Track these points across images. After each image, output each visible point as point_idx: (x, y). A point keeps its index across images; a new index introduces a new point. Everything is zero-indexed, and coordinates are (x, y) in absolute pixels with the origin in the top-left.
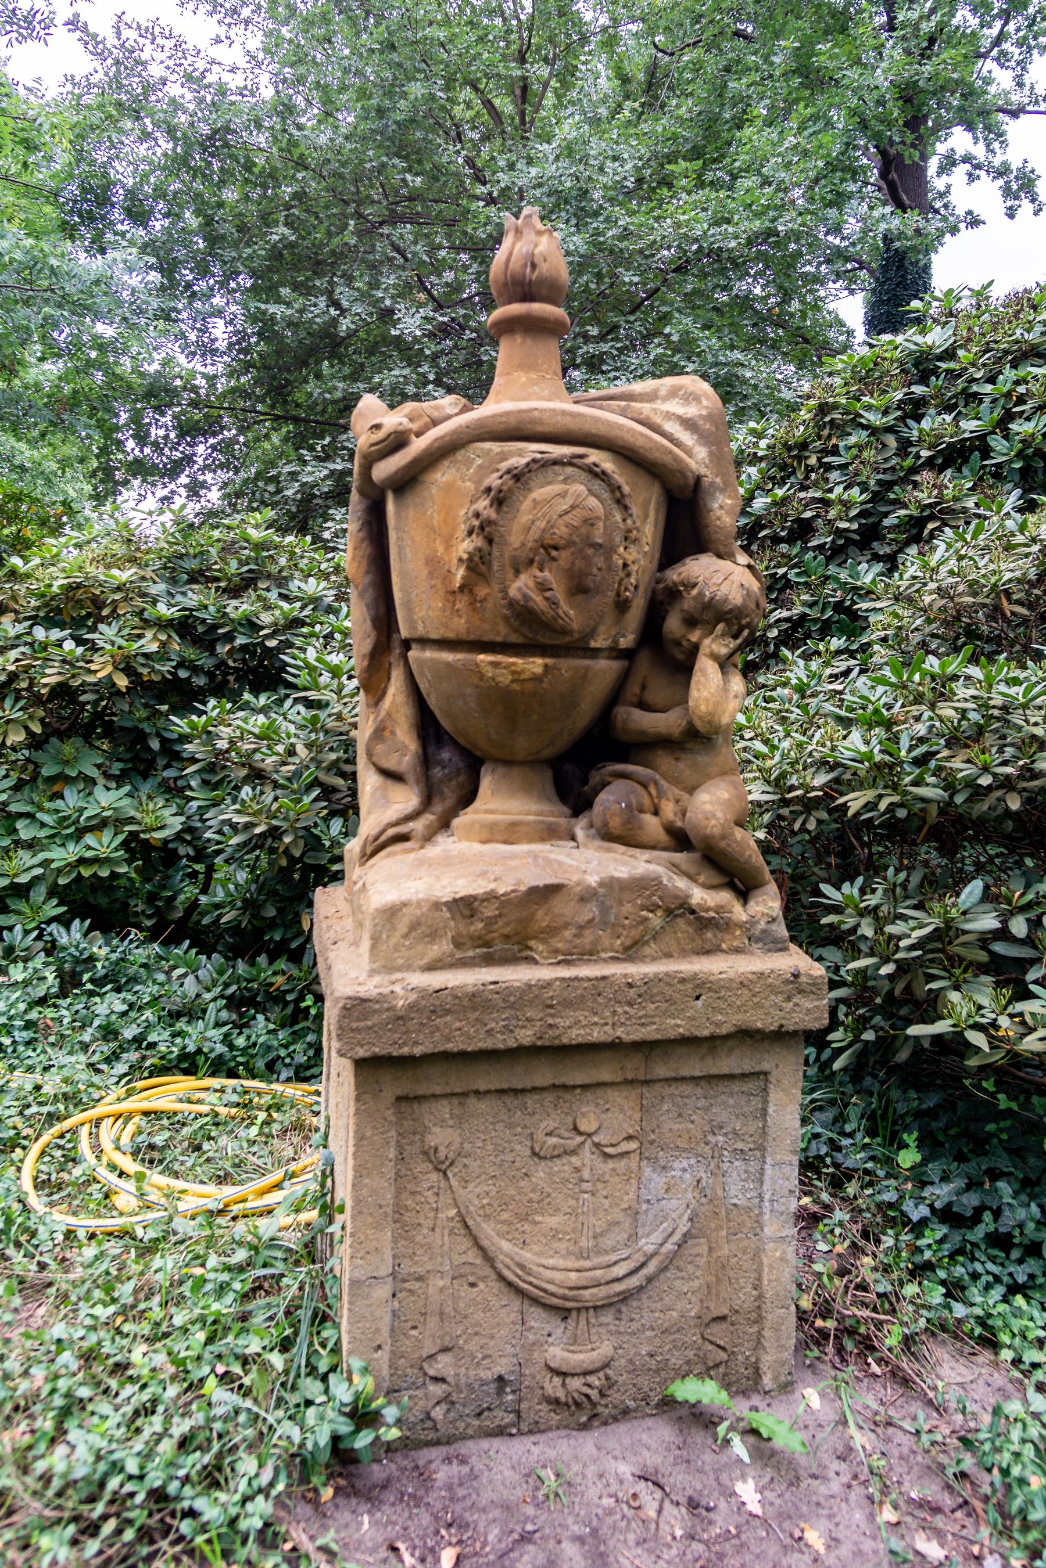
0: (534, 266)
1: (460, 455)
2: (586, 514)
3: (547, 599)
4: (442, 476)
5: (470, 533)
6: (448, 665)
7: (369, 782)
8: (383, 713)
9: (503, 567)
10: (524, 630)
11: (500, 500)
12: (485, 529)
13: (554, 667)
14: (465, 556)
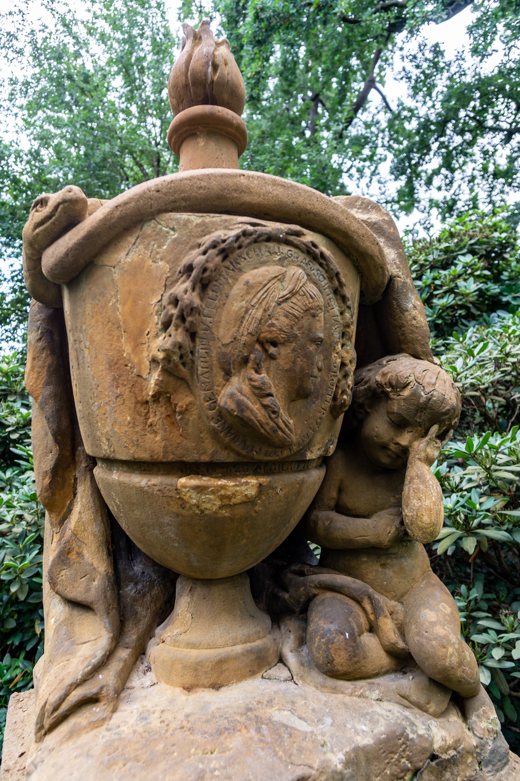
0: (215, 67)
1: (149, 228)
2: (308, 301)
3: (265, 407)
4: (126, 256)
5: (166, 326)
6: (141, 490)
7: (54, 611)
8: (68, 533)
9: (210, 368)
10: (237, 446)
11: (204, 282)
12: (186, 319)
13: (270, 487)
14: (161, 355)
